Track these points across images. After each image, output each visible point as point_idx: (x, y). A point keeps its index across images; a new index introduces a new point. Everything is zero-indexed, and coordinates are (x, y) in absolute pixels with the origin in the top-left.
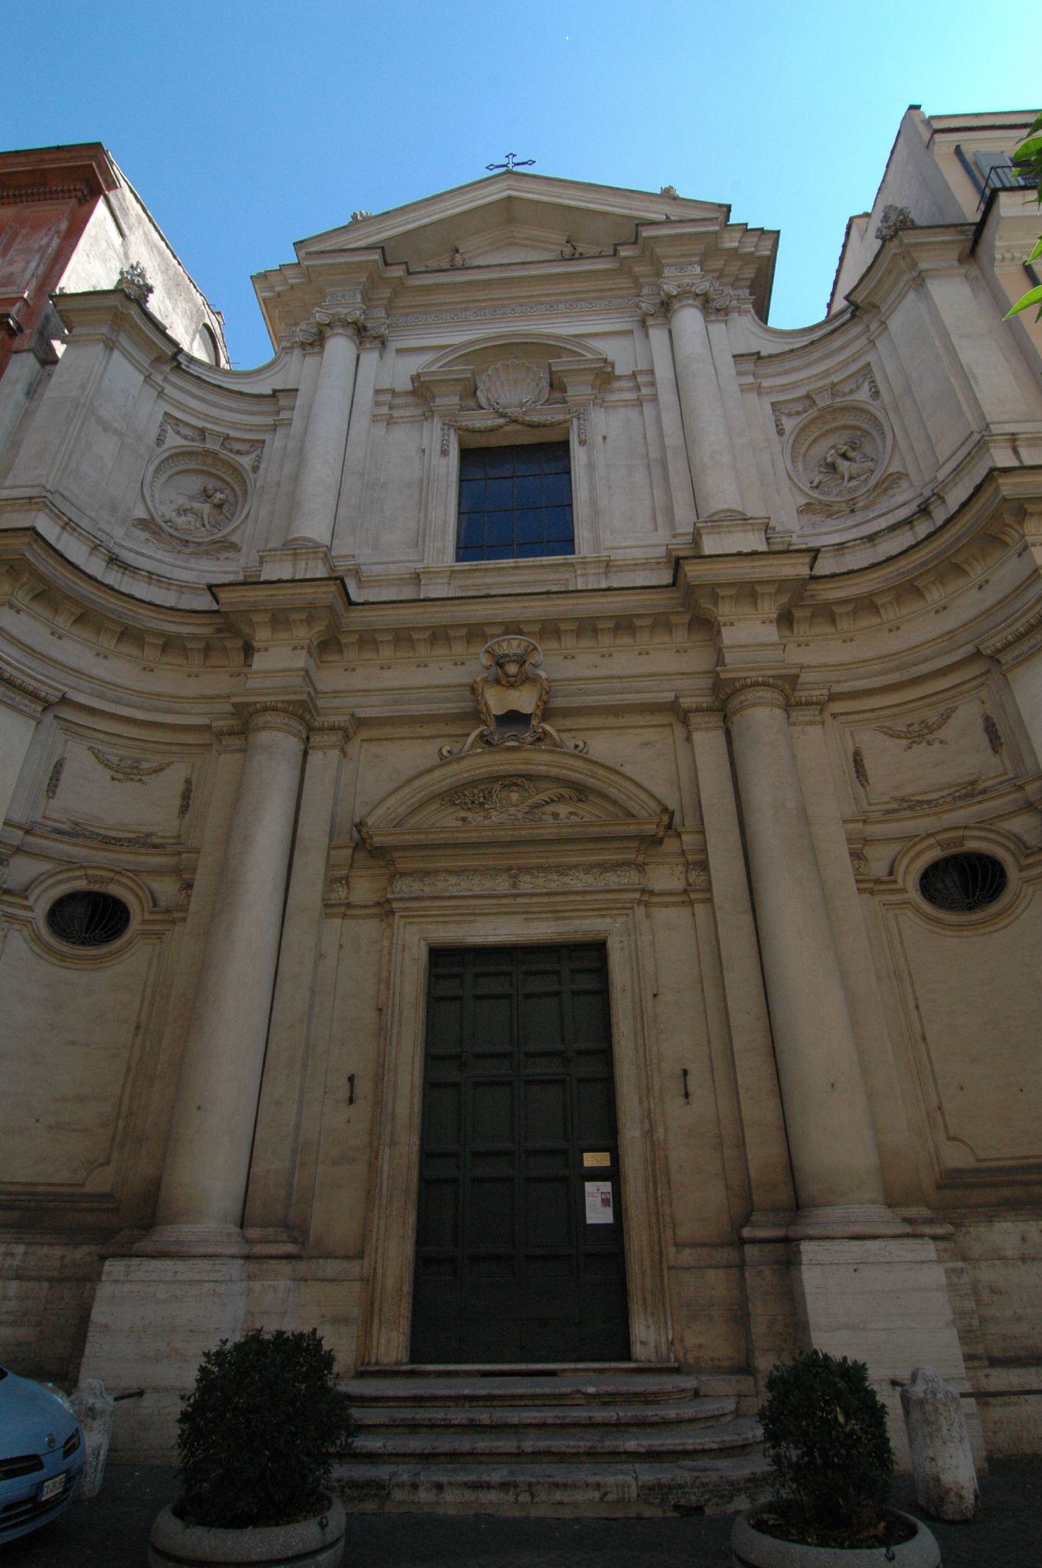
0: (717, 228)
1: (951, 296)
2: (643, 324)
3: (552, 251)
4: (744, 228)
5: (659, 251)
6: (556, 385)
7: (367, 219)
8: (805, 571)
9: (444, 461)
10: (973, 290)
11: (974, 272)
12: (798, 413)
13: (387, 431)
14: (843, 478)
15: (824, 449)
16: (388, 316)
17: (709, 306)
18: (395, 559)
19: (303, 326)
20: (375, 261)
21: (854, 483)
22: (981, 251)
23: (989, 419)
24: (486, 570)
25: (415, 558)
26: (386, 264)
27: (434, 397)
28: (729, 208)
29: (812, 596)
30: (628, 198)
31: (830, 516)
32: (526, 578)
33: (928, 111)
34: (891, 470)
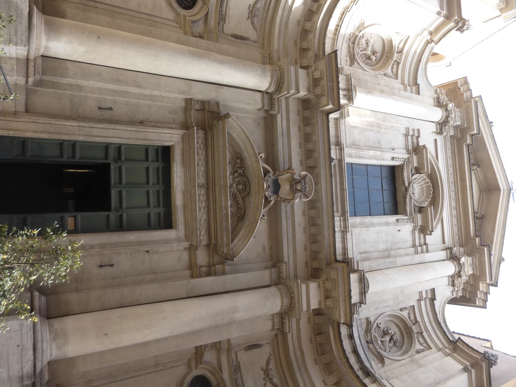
4: (486, 294)
6: (421, 210)
12: (409, 317)
14: (382, 337)
15: (394, 330)
21: (380, 343)
25: (348, 144)
34: (385, 359)
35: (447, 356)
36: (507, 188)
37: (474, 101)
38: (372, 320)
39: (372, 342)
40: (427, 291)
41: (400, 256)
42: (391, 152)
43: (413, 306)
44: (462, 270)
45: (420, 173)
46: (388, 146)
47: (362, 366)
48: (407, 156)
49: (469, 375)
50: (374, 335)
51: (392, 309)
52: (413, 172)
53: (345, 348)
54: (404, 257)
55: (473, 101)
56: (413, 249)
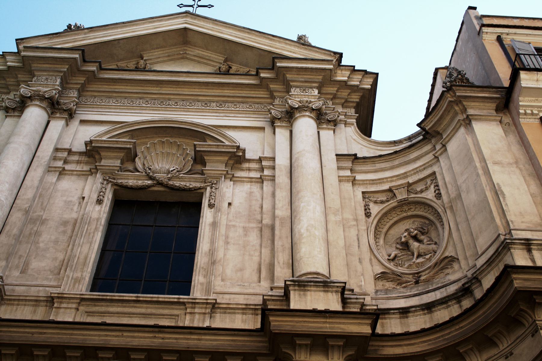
0: (331, 67)
1: (489, 134)
2: (273, 122)
3: (213, 66)
4: (353, 70)
5: (289, 76)
6: (199, 159)
7: (78, 28)
8: (366, 330)
9: (98, 208)
10: (505, 132)
11: (507, 119)
12: (382, 202)
13: (58, 179)
14: (413, 255)
15: (400, 231)
16: (80, 96)
17: (320, 117)
18: (39, 282)
19: (11, 96)
20: (75, 59)
21: (421, 260)
22: (512, 106)
23: (512, 227)
24: (112, 301)
25: (55, 283)
26: (84, 61)
27: (101, 159)
28: (341, 55)
29: (376, 350)
30: (271, 40)
31: (400, 284)
32: (143, 311)
33: (481, 11)
34: (447, 254)
35: (446, 150)
36: (183, 17)
37: (24, 51)
38: (379, 269)
39: (418, 273)
40: (339, 168)
41: (274, 207)
42: (87, 203)
43: (363, 193)
44: (310, 105)
45: (136, 155)
46: (75, 208)
47: (455, 299)
48: (98, 175)
49: (476, 120)
50: (408, 268)
51: (361, 233)
52: (131, 168)
53: (419, 329)
54: (277, 202)
55: (23, 54)
56: (265, 183)
